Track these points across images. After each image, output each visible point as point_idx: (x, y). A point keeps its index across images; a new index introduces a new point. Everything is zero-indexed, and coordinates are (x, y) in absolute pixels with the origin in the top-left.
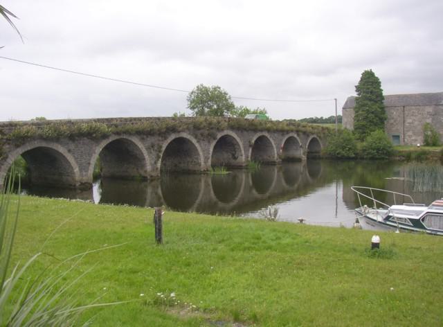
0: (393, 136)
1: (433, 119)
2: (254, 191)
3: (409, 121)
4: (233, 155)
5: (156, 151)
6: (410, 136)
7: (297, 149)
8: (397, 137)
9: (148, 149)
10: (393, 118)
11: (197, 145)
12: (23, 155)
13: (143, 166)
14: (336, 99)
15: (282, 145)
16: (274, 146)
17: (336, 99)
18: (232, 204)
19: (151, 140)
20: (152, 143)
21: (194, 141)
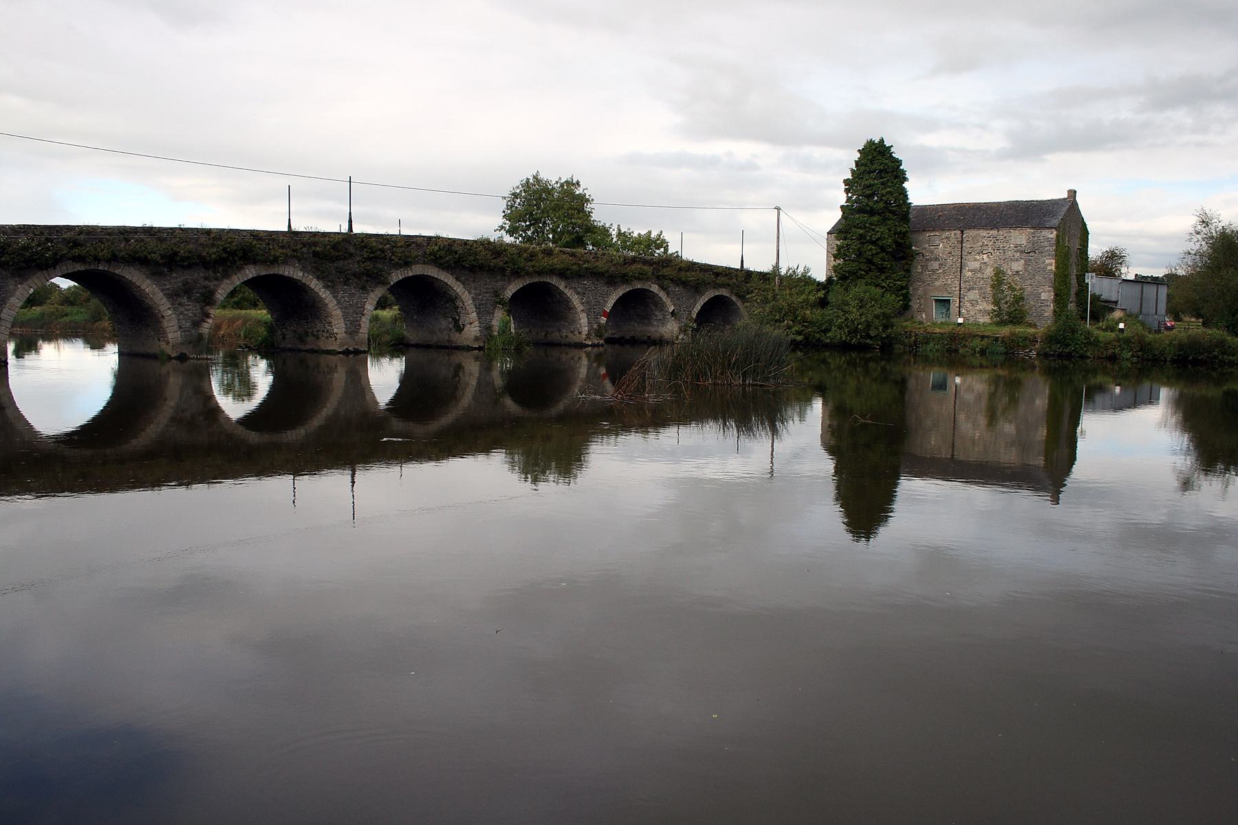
0: (936, 300)
1: (1027, 264)
2: (509, 403)
3: (973, 265)
4: (456, 322)
5: (197, 301)
6: (973, 303)
7: (663, 322)
8: (945, 303)
9: (173, 296)
10: (936, 259)
11: (324, 294)
12: (388, 289)
13: (160, 333)
14: (778, 209)
15: (608, 307)
16: (579, 307)
17: (350, 177)
18: (434, 426)
19: (178, 279)
20: (185, 283)
21: (314, 284)
